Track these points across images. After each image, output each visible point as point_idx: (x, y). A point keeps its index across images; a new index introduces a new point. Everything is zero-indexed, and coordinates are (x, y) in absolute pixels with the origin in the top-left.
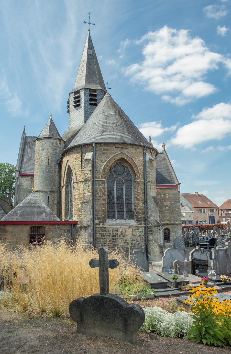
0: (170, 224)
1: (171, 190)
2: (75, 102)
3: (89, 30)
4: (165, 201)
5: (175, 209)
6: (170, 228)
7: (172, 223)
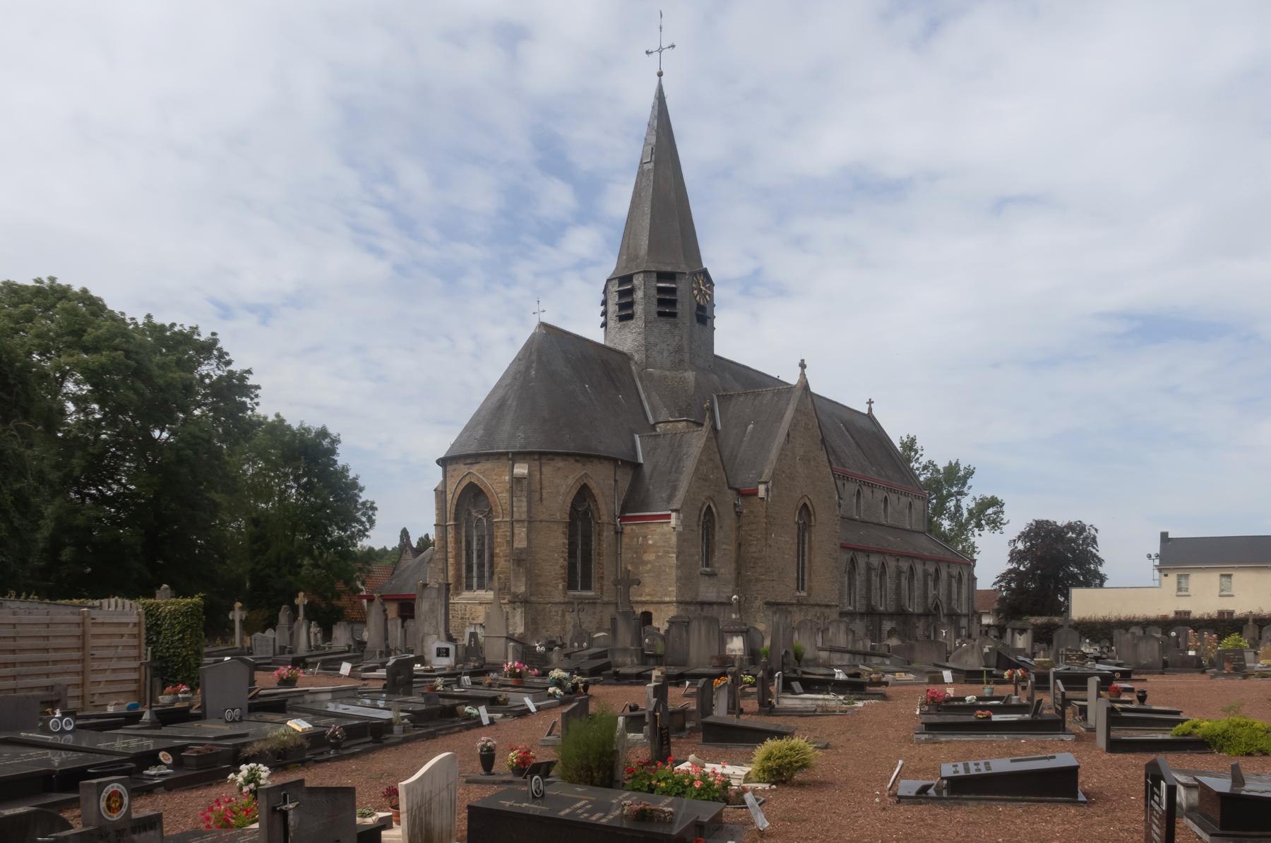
0: (652, 603)
1: (657, 526)
2: (622, 307)
3: (660, 74)
4: (645, 552)
5: (663, 568)
6: (652, 611)
7: (656, 599)
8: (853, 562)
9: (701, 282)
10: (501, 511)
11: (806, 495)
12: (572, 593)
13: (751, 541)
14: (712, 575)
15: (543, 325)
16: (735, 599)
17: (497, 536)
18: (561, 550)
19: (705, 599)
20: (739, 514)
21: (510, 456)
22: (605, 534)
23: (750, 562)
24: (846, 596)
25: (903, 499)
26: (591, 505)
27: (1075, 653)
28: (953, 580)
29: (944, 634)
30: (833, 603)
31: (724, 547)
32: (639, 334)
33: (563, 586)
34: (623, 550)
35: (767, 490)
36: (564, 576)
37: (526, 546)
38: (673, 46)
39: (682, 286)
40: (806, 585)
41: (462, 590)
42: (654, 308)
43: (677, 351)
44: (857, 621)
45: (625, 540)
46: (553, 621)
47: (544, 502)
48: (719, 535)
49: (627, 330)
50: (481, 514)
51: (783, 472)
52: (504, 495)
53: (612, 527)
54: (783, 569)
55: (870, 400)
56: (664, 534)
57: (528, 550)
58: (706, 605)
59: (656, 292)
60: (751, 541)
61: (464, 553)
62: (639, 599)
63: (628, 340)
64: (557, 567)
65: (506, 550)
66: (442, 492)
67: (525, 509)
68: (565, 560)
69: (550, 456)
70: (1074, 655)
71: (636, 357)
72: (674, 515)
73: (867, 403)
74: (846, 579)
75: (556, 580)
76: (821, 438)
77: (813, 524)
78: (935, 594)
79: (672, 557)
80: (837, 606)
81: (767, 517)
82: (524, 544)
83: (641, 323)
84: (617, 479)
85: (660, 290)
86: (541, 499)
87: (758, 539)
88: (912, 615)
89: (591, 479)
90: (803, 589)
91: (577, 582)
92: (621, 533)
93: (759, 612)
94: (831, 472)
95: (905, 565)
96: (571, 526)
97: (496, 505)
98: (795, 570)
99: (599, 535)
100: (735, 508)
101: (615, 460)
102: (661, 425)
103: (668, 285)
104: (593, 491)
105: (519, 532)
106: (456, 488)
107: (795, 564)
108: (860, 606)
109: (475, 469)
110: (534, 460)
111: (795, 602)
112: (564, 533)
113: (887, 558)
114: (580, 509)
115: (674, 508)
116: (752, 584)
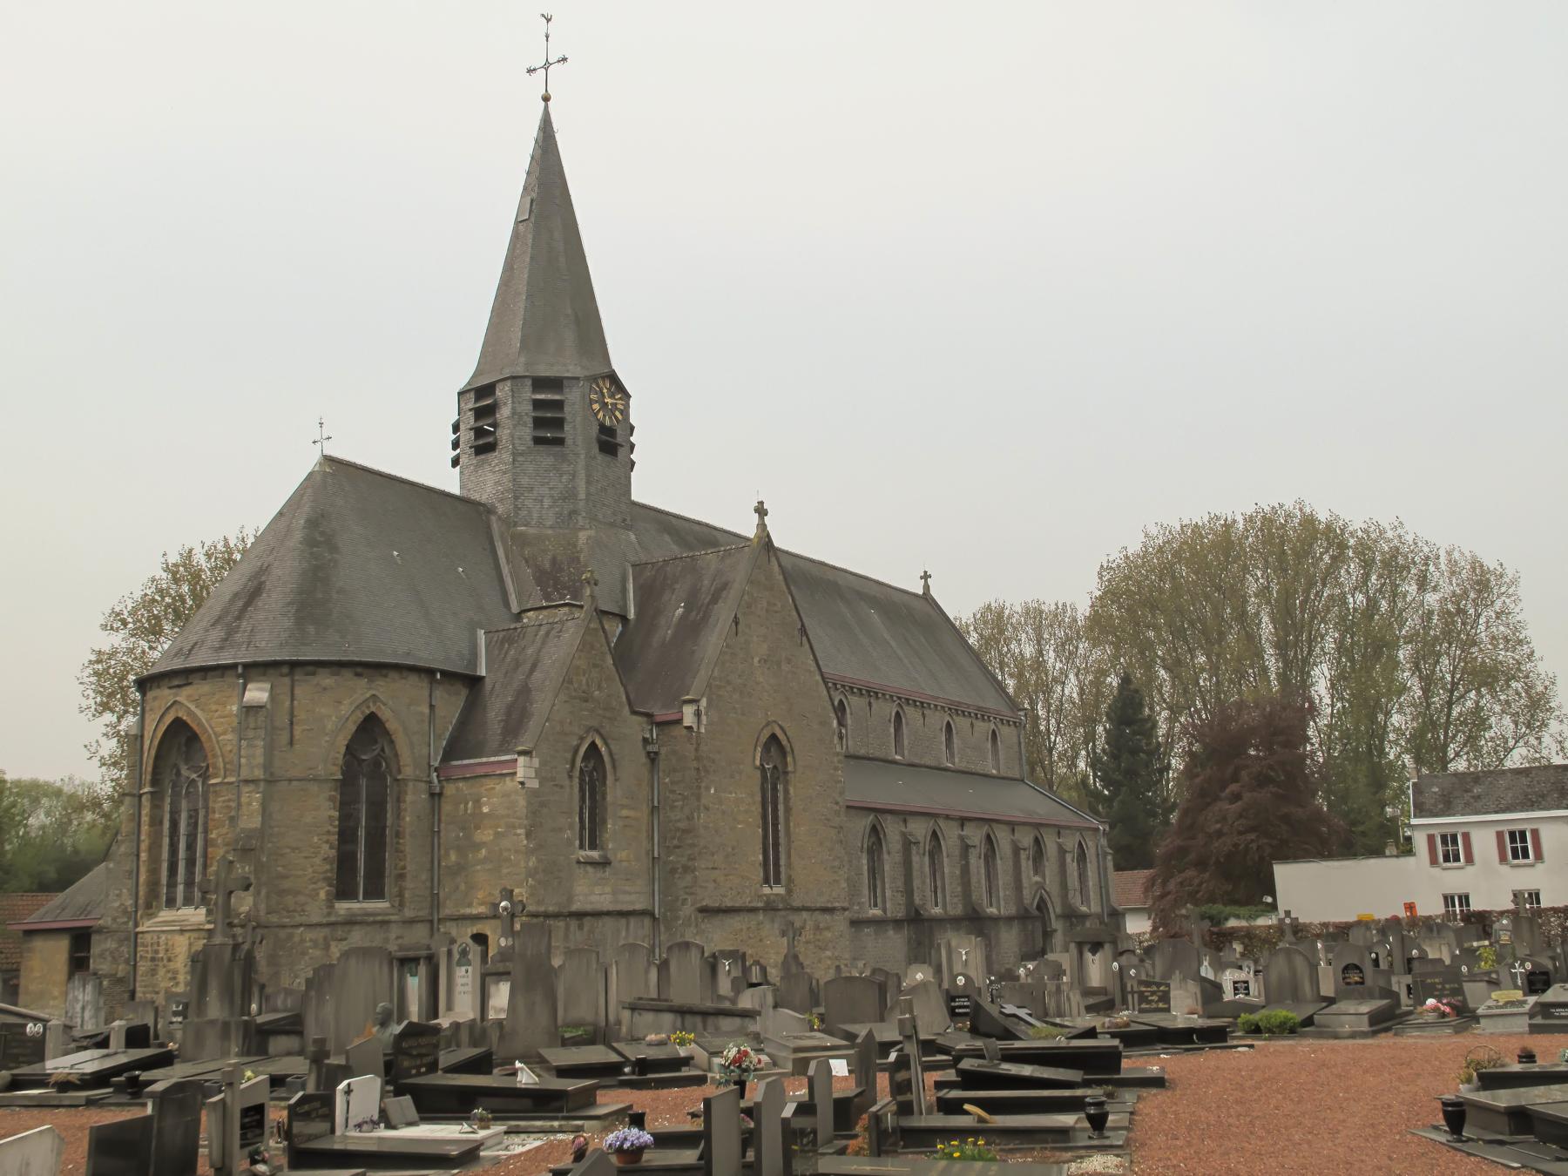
3: (546, 99)
4: (477, 827)
5: (505, 854)
6: (489, 933)
8: (875, 830)
9: (605, 391)
10: (222, 765)
11: (775, 722)
12: (343, 907)
13: (674, 801)
14: (604, 863)
15: (329, 460)
16: (505, 909)
17: (213, 808)
18: (326, 829)
19: (588, 908)
20: (653, 758)
21: (240, 670)
22: (409, 798)
23: (674, 838)
24: (866, 892)
25: (979, 725)
26: (386, 749)
27: (1155, 988)
28: (1069, 858)
29: (964, 958)
30: (837, 905)
31: (625, 812)
32: (505, 473)
33: (328, 893)
34: (443, 825)
35: (698, 714)
36: (329, 875)
37: (259, 826)
38: (564, 59)
39: (572, 398)
40: (783, 876)
41: (159, 909)
42: (527, 432)
43: (566, 498)
44: (891, 933)
45: (447, 808)
46: (307, 958)
47: (297, 747)
48: (614, 792)
49: (487, 468)
50: (195, 773)
51: (729, 683)
52: (229, 737)
53: (423, 786)
54: (733, 849)
55: (926, 572)
56: (506, 795)
57: (262, 833)
58: (589, 918)
59: (531, 408)
60: (674, 801)
61: (166, 841)
62: (468, 911)
63: (490, 484)
64: (317, 861)
65: (227, 834)
66: (136, 736)
67: (260, 760)
68: (331, 848)
69: (310, 668)
70: (1153, 993)
71: (500, 509)
72: (521, 760)
73: (921, 578)
74: (865, 861)
75: (315, 883)
76: (799, 627)
77: (790, 768)
78: (1037, 883)
79: (519, 835)
80: (844, 909)
81: (697, 759)
82: (255, 822)
83: (507, 457)
84: (433, 703)
85: (537, 404)
86: (291, 743)
87: (685, 798)
88: (995, 920)
89: (385, 704)
90: (777, 881)
91: (356, 885)
92: (440, 795)
93: (690, 926)
94: (821, 681)
95: (975, 835)
96: (347, 784)
97: (214, 756)
98: (759, 847)
99: (399, 800)
100: (645, 747)
101: (429, 672)
102: (530, 614)
103: (550, 397)
104: (387, 725)
105: (247, 800)
106: (155, 730)
107: (760, 840)
108: (895, 908)
109: (183, 695)
110: (282, 675)
111: (760, 905)
112: (331, 799)
113: (941, 823)
114: (364, 757)
115: (520, 748)
116: (677, 876)
